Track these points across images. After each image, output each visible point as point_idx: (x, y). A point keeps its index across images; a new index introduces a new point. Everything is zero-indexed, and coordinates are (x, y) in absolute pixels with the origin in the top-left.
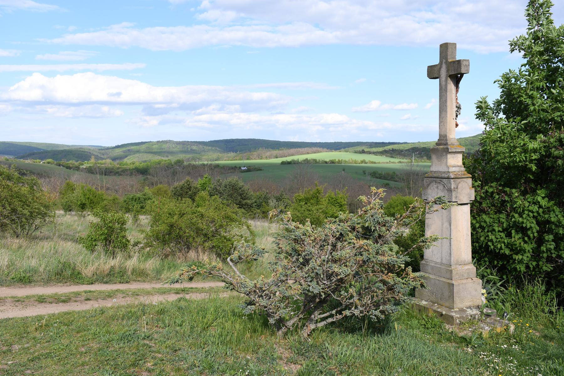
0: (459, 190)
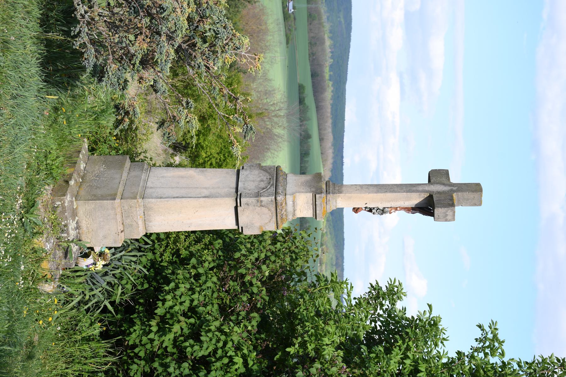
0: (258, 209)
